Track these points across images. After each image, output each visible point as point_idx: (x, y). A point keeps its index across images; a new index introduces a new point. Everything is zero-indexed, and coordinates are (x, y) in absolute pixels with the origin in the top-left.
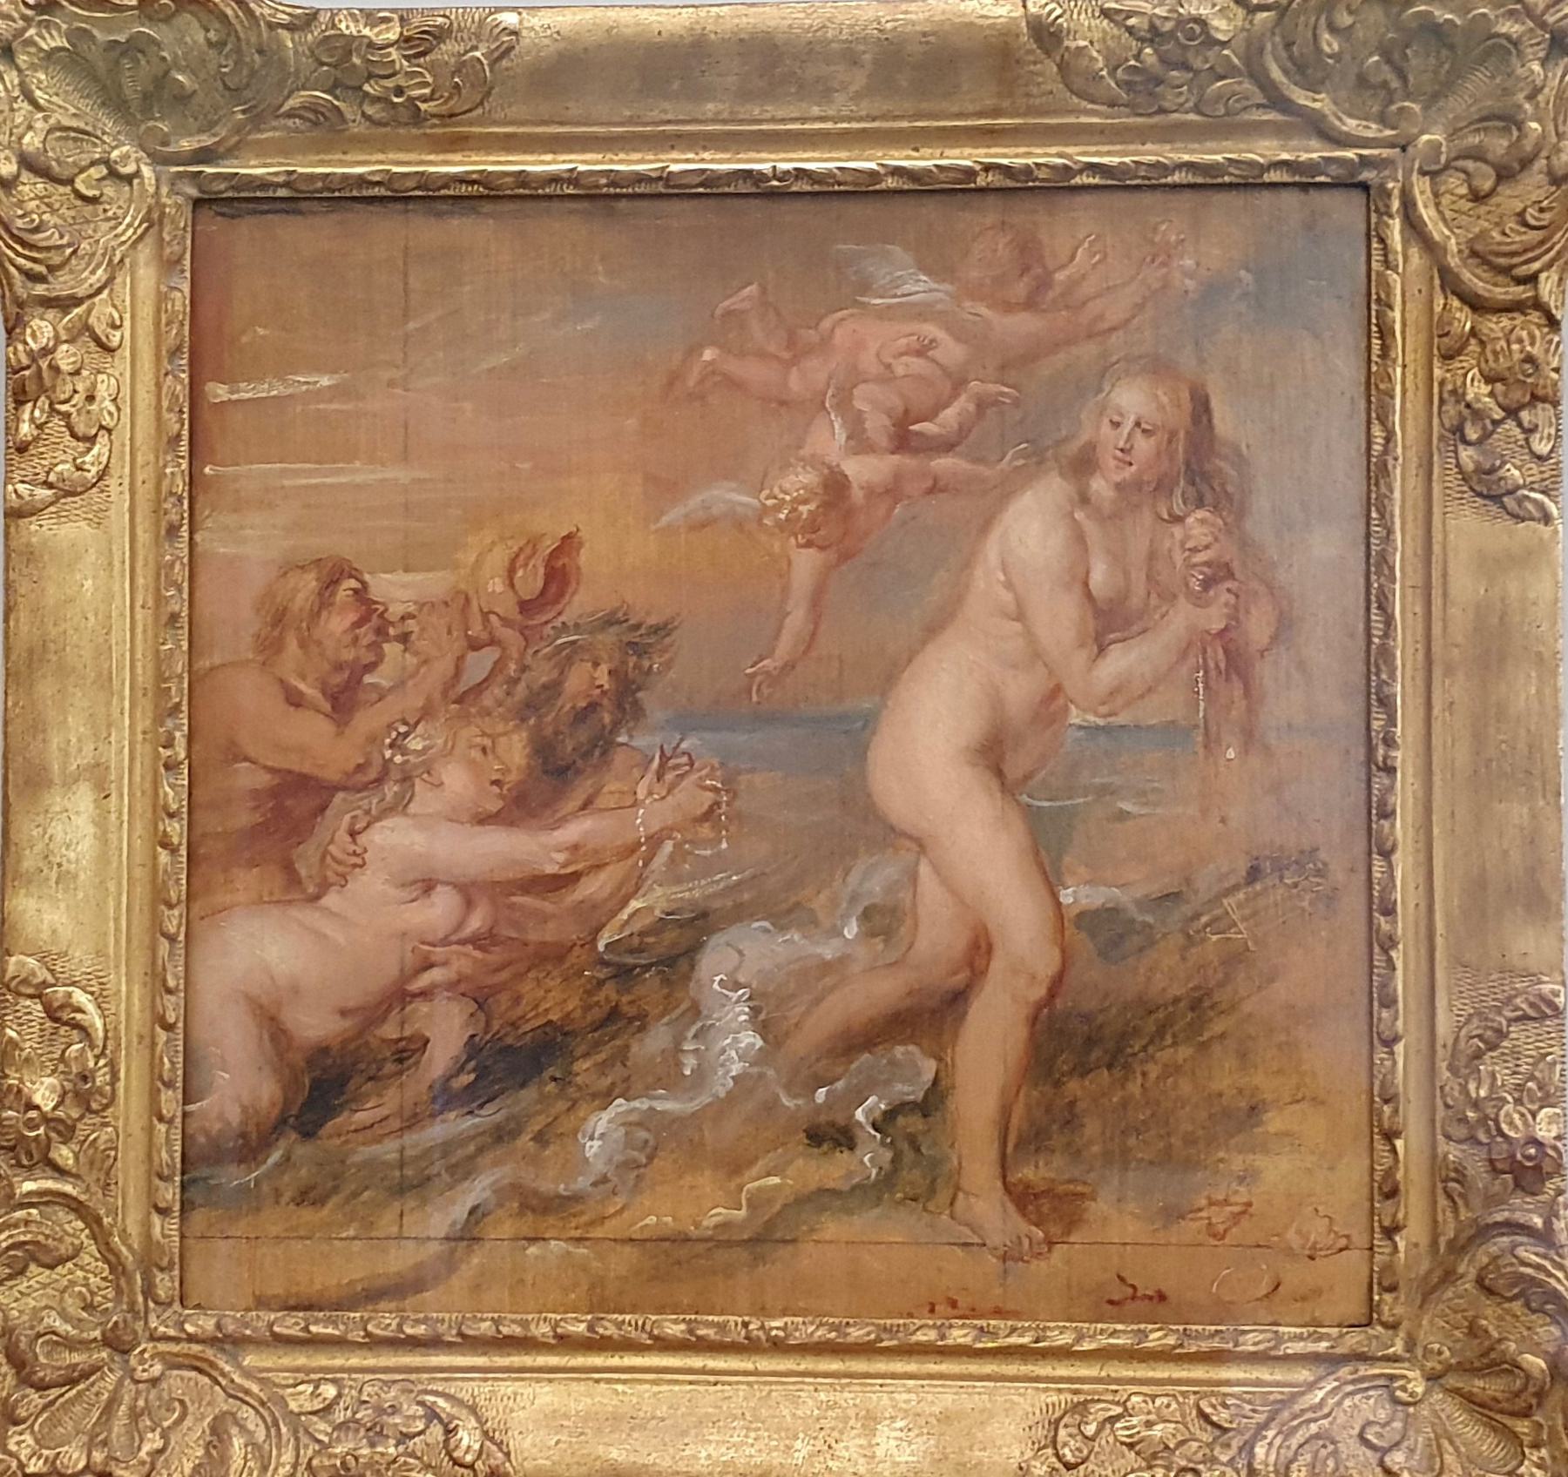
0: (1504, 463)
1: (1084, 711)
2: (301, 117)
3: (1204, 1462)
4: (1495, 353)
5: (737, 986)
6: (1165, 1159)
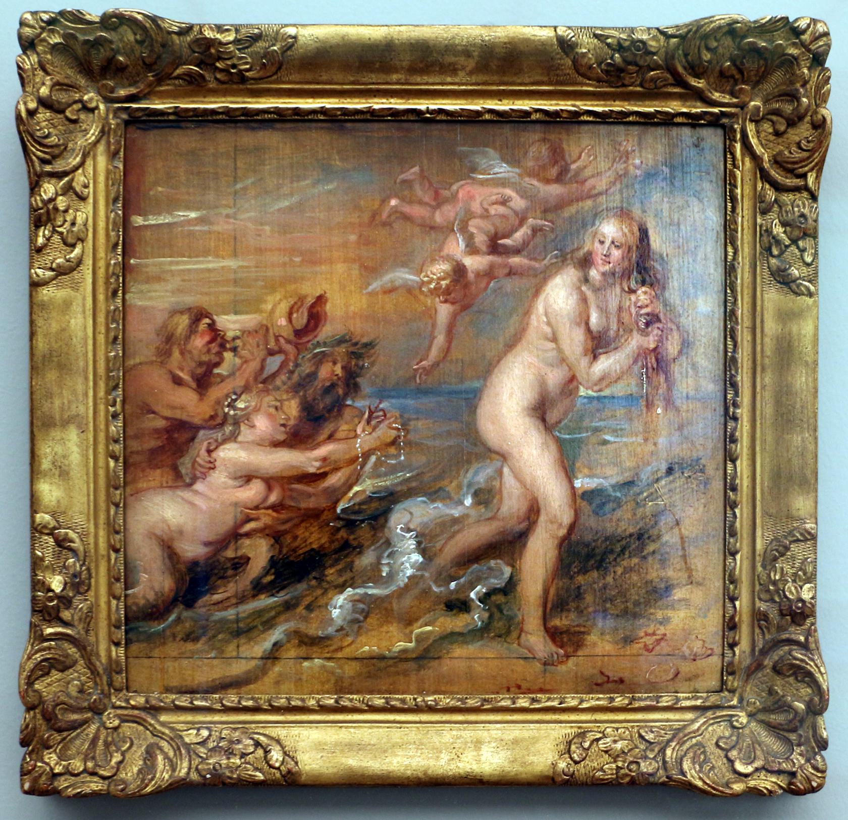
0: (790, 267)
1: (587, 389)
2: (182, 79)
3: (641, 758)
4: (787, 212)
5: (409, 530)
6: (625, 613)
